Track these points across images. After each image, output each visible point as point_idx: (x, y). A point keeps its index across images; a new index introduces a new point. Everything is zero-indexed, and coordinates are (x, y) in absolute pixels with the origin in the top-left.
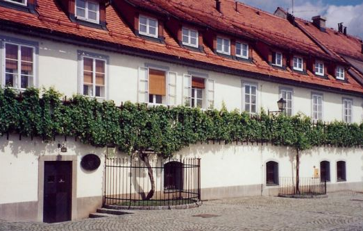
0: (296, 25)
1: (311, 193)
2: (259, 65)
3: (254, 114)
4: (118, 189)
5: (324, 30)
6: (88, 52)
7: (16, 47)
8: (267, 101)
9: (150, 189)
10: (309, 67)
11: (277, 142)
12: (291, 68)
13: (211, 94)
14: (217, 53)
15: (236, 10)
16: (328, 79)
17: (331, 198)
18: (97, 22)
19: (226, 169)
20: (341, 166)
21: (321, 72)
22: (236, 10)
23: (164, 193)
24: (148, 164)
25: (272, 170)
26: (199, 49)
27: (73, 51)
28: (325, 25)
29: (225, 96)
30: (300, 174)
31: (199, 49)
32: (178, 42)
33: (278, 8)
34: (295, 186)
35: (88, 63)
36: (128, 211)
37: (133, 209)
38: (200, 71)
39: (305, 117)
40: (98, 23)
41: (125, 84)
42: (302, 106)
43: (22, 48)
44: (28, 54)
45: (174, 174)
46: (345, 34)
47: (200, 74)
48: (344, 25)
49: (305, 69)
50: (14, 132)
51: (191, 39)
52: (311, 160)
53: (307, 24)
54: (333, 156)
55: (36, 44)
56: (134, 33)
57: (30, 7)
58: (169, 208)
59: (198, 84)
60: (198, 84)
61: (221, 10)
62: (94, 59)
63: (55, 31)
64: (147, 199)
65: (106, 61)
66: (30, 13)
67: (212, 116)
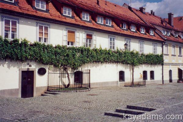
0: (132, 11)
1: (139, 85)
5: (145, 13)
7: (9, 21)
8: (120, 44)
11: (124, 62)
13: (95, 41)
14: (98, 23)
16: (146, 35)
17: (148, 87)
18: (45, 9)
19: (102, 74)
20: (152, 73)
21: (143, 32)
22: (106, 4)
23: (74, 85)
24: (67, 72)
25: (122, 75)
26: (90, 22)
27: (34, 22)
29: (101, 42)
30: (134, 77)
31: (90, 22)
33: (124, 4)
34: (132, 82)
36: (59, 93)
37: (61, 92)
38: (90, 31)
40: (45, 10)
41: (57, 37)
42: (135, 46)
43: (12, 21)
44: (14, 24)
45: (78, 76)
46: (154, 15)
47: (90, 32)
48: (153, 11)
50: (9, 58)
51: (86, 17)
52: (139, 70)
53: (137, 11)
54: (148, 69)
55: (18, 19)
56: (61, 14)
57: (15, 3)
58: (77, 92)
59: (89, 37)
60: (89, 37)
62: (44, 26)
65: (49, 27)
66: (15, 6)
67: (95, 51)
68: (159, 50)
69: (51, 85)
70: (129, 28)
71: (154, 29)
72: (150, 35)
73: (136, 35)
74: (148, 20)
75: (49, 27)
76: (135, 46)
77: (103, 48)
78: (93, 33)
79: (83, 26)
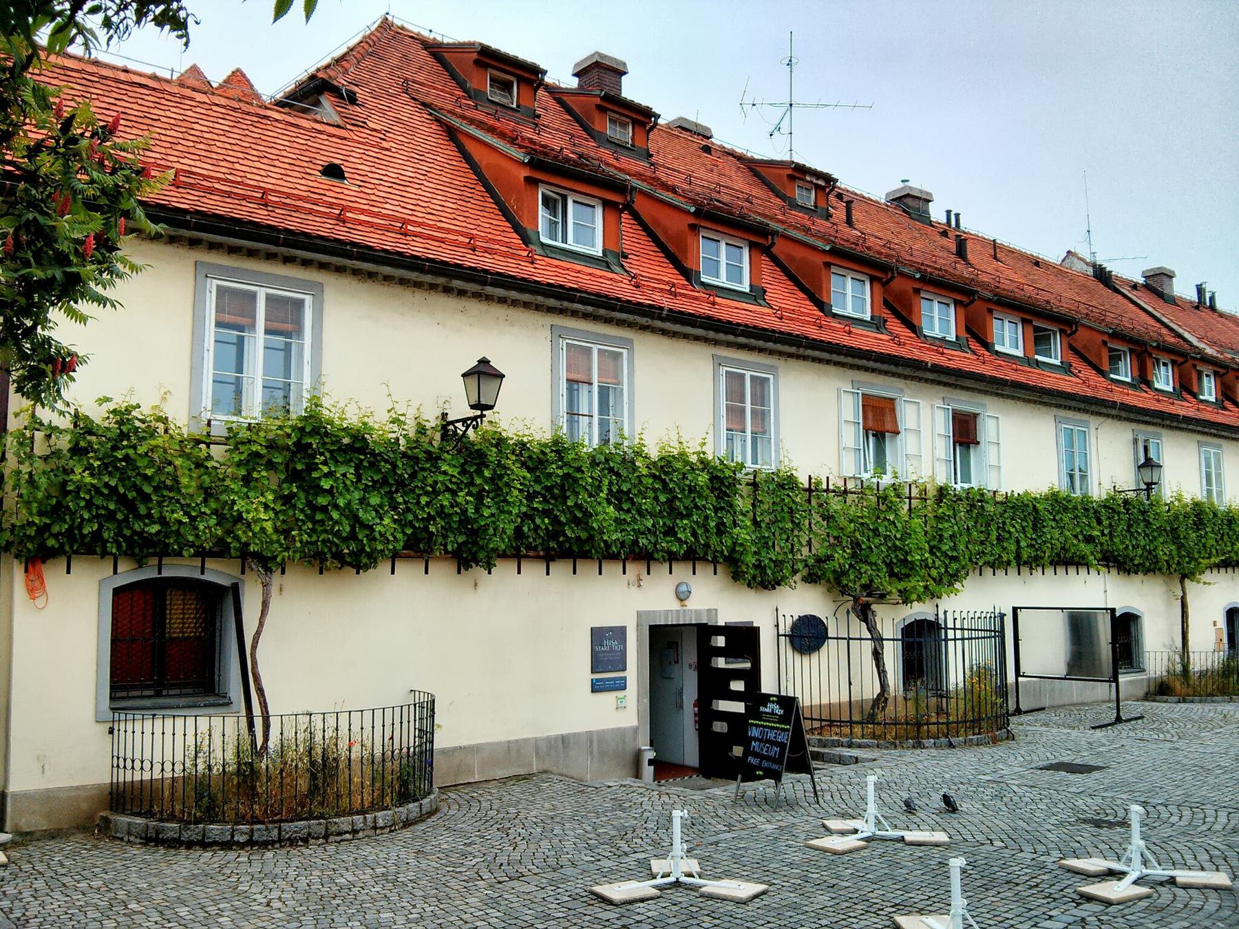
0: (1116, 291)
3: (966, 486)
4: (122, 746)
5: (1172, 301)
7: (253, 296)
8: (1110, 464)
9: (878, 690)
12: (1149, 384)
13: (993, 449)
14: (997, 353)
15: (995, 258)
16: (1225, 408)
18: (597, 251)
21: (1056, 358)
22: (995, 258)
23: (905, 699)
24: (871, 628)
26: (957, 345)
28: (1171, 285)
29: (1024, 456)
30: (1190, 636)
31: (957, 345)
32: (914, 328)
33: (1069, 252)
34: (1179, 668)
36: (846, 752)
37: (860, 746)
40: (747, 290)
41: (812, 432)
42: (1184, 473)
43: (269, 298)
46: (1212, 308)
47: (966, 402)
48: (1208, 288)
49: (1177, 387)
50: (732, 569)
53: (1135, 286)
55: (317, 290)
56: (822, 310)
57: (610, 259)
58: (951, 746)
59: (965, 433)
60: (965, 433)
61: (969, 256)
62: (595, 348)
63: (934, 365)
65: (308, 300)
66: (613, 272)
67: (497, 446)
69: (148, 723)
70: (1143, 380)
72: (1202, 401)
73: (1183, 408)
75: (308, 300)
76: (1184, 473)
78: (984, 406)
79: (937, 369)
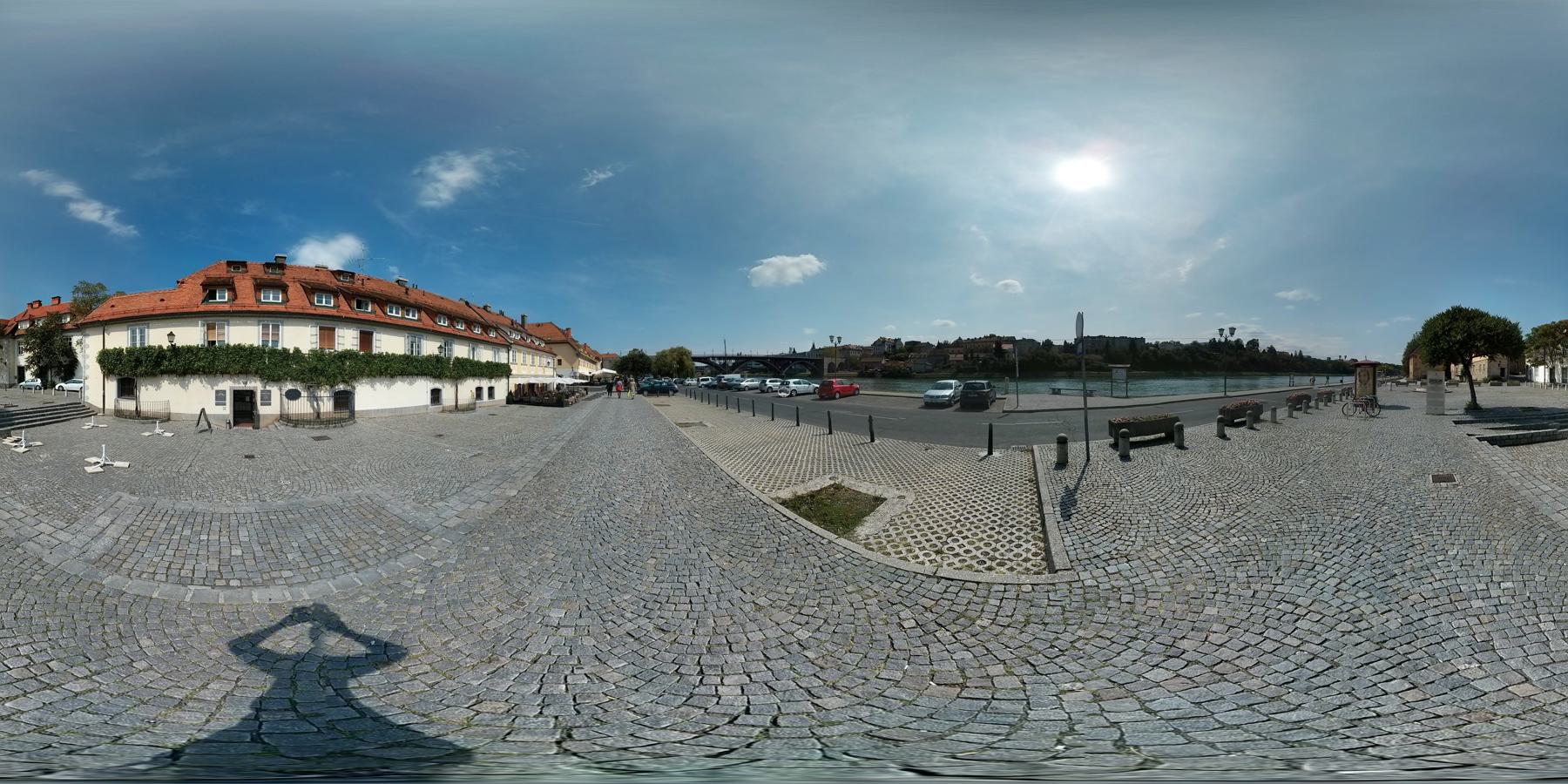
1: (470, 408)
2: (345, 309)
6: (266, 320)
8: (430, 347)
10: (452, 324)
11: (438, 376)
17: (478, 411)
19: (370, 396)
20: (491, 389)
25: (436, 395)
27: (255, 320)
35: (265, 327)
38: (449, 337)
39: (1110, 378)
44: (276, 327)
45: (344, 401)
47: (367, 328)
51: (478, 331)
52: (468, 388)
54: (485, 384)
64: (318, 419)
68: (502, 357)
71: (496, 329)
74: (488, 318)
77: (1058, 342)
